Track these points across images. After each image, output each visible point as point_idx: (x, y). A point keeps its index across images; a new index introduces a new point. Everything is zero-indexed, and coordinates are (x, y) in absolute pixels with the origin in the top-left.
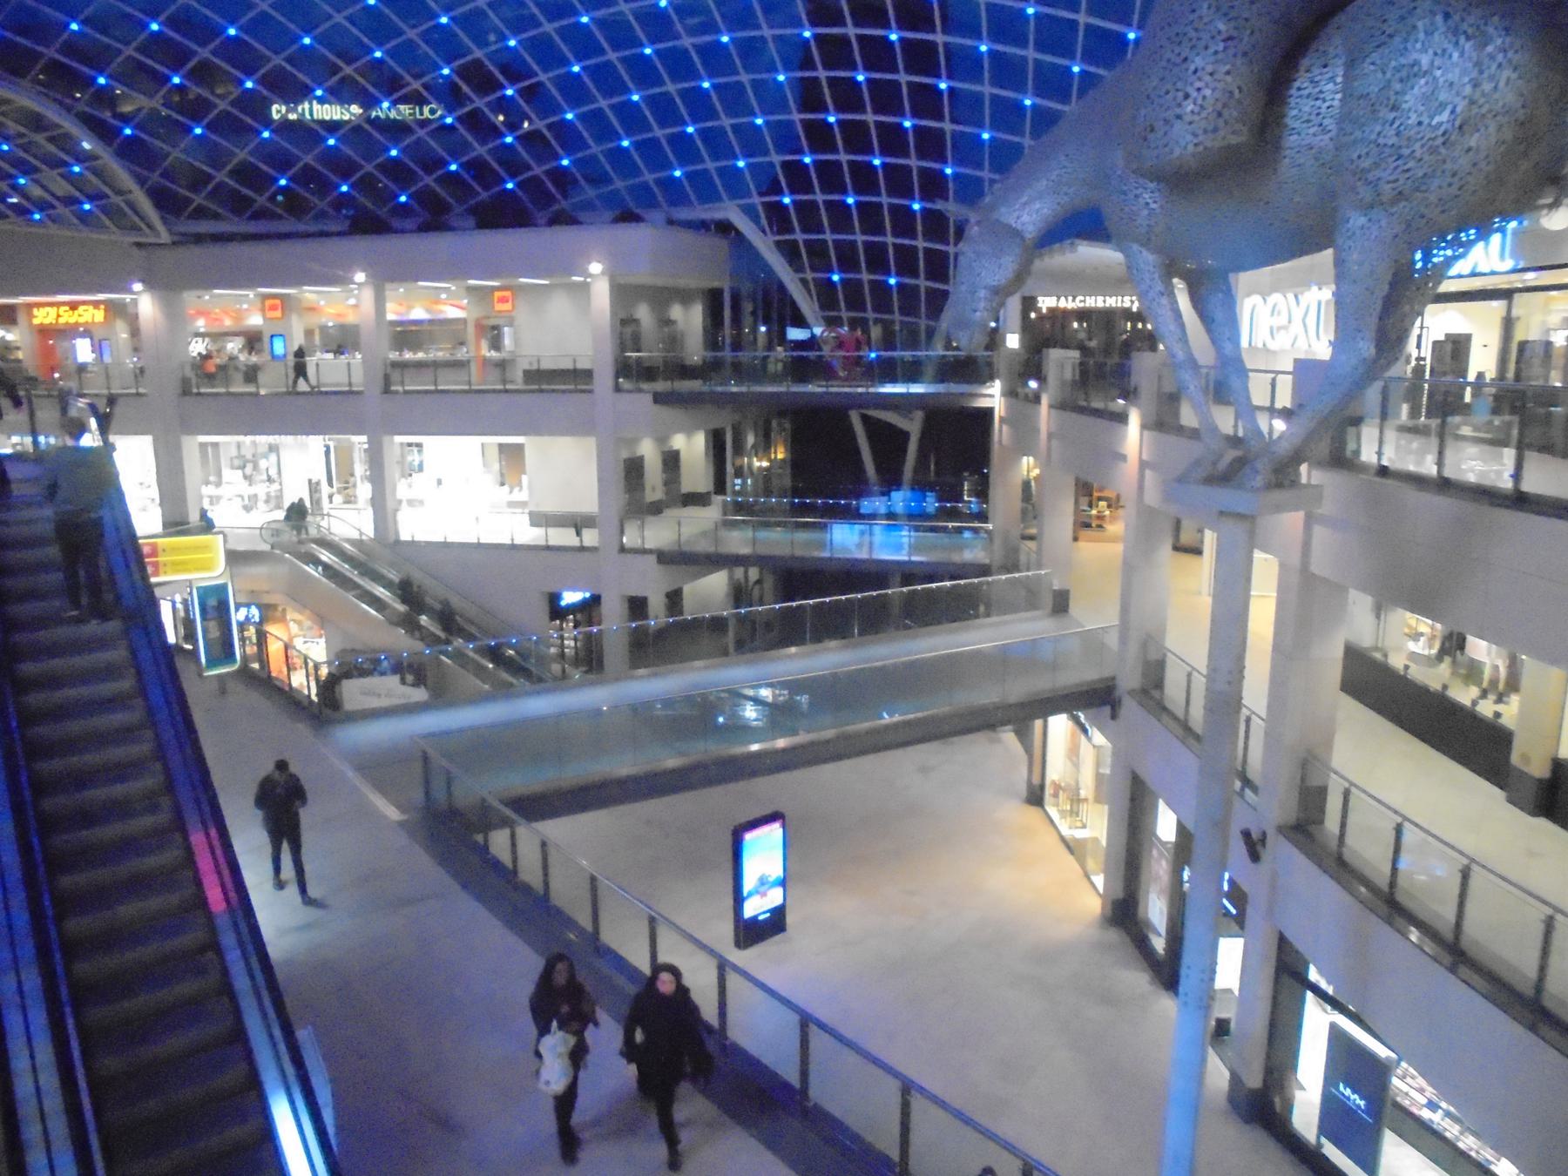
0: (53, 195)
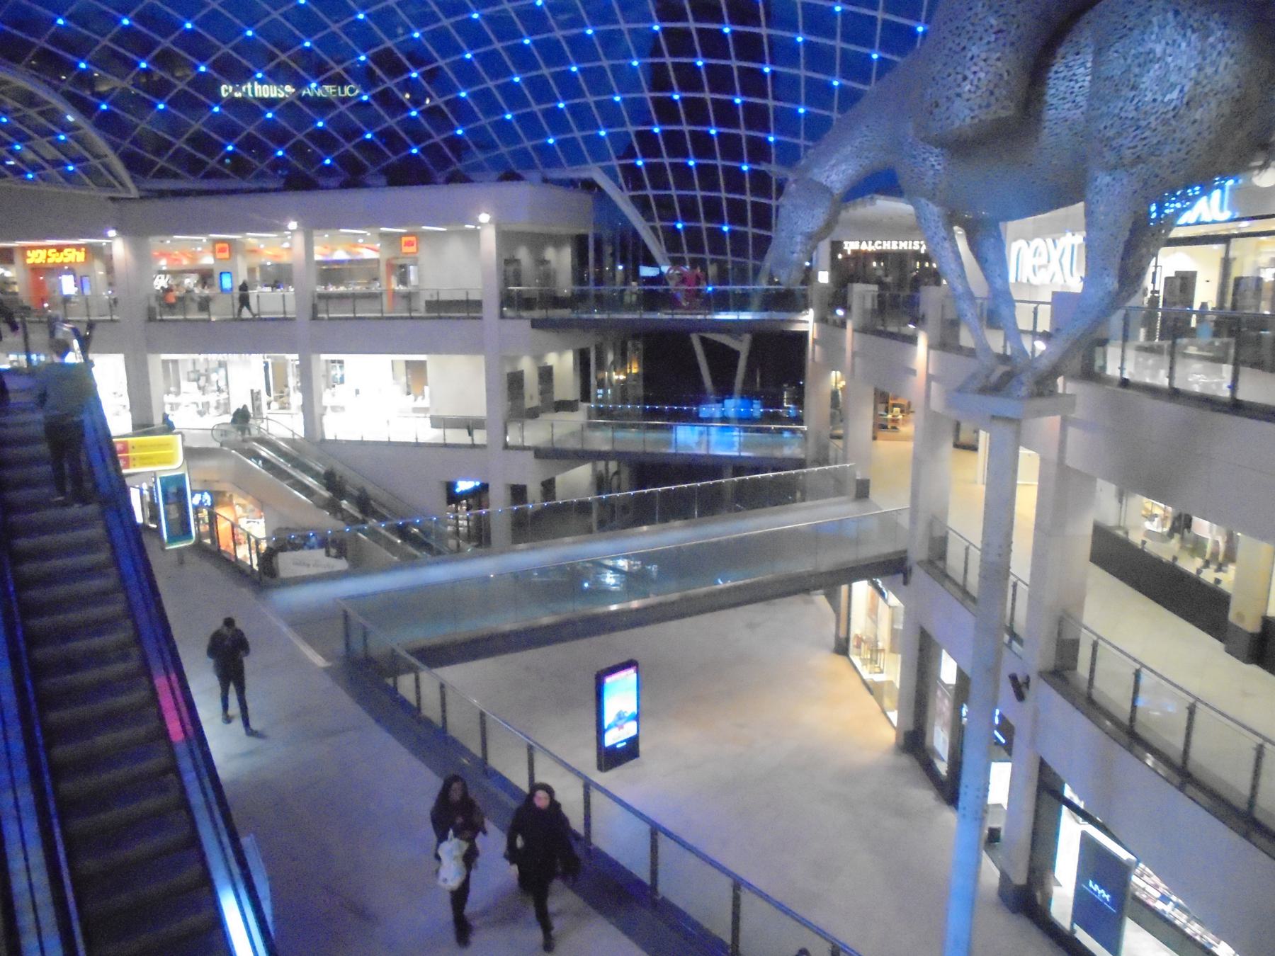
0: (43, 158)
